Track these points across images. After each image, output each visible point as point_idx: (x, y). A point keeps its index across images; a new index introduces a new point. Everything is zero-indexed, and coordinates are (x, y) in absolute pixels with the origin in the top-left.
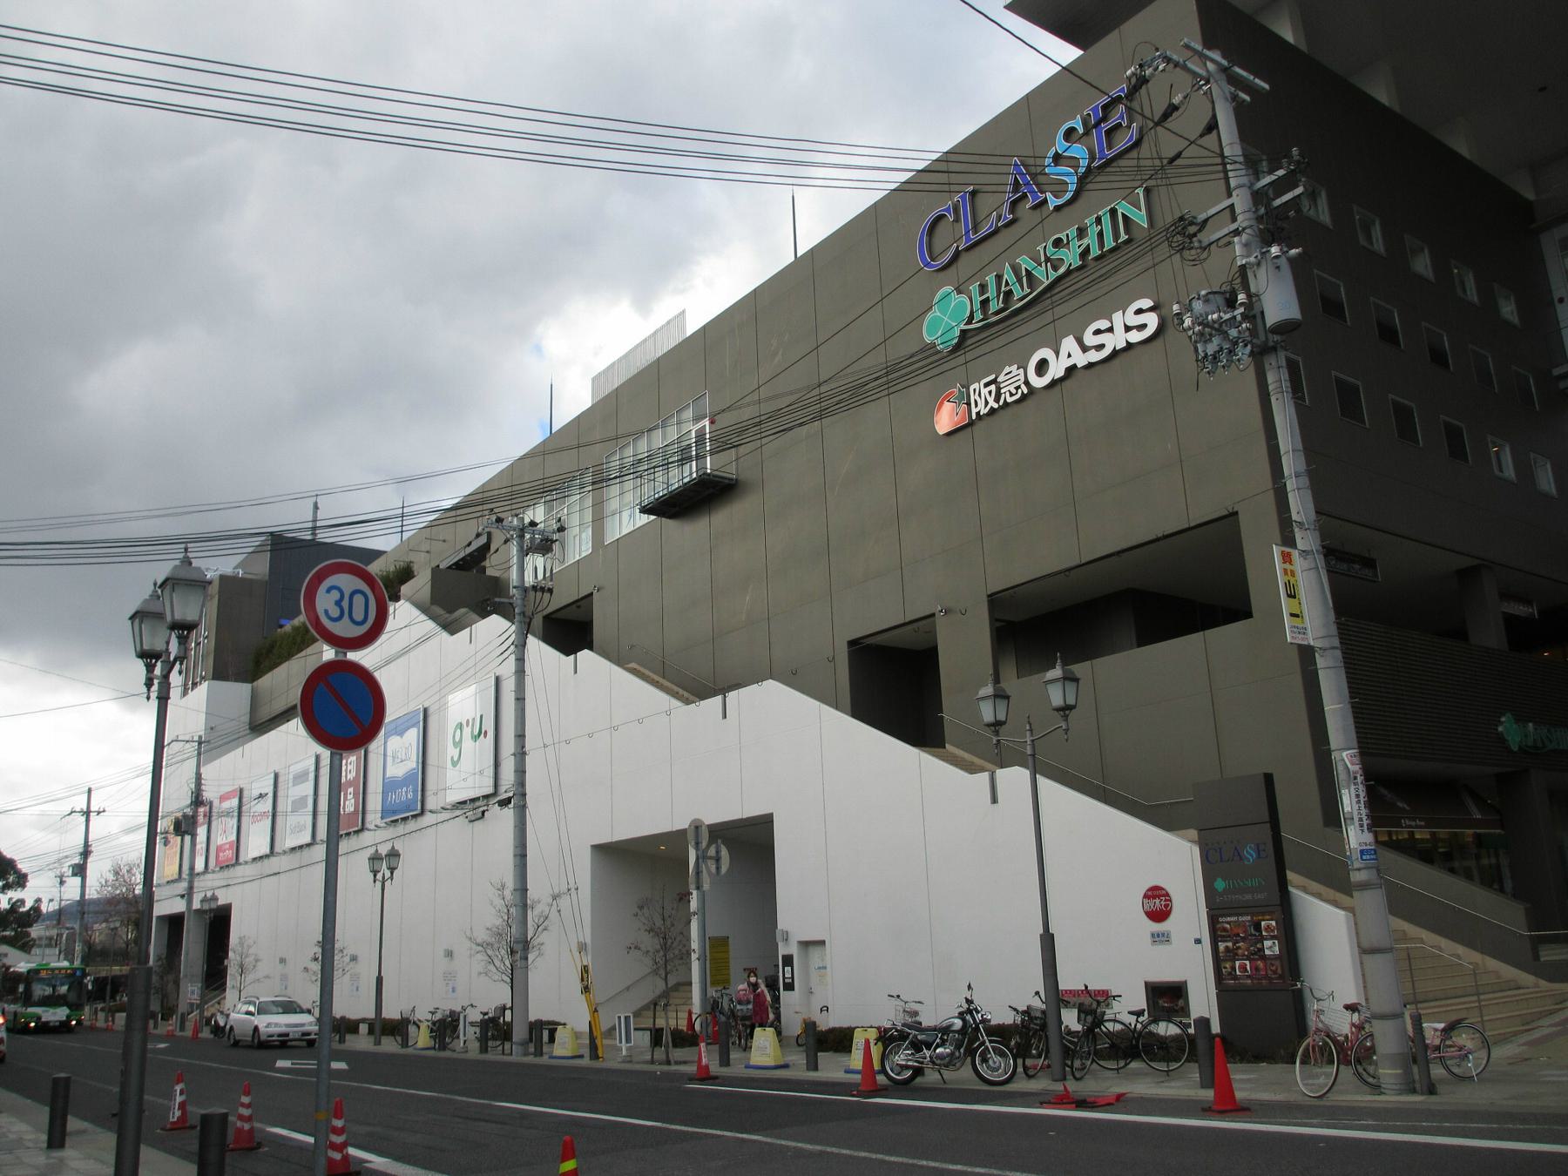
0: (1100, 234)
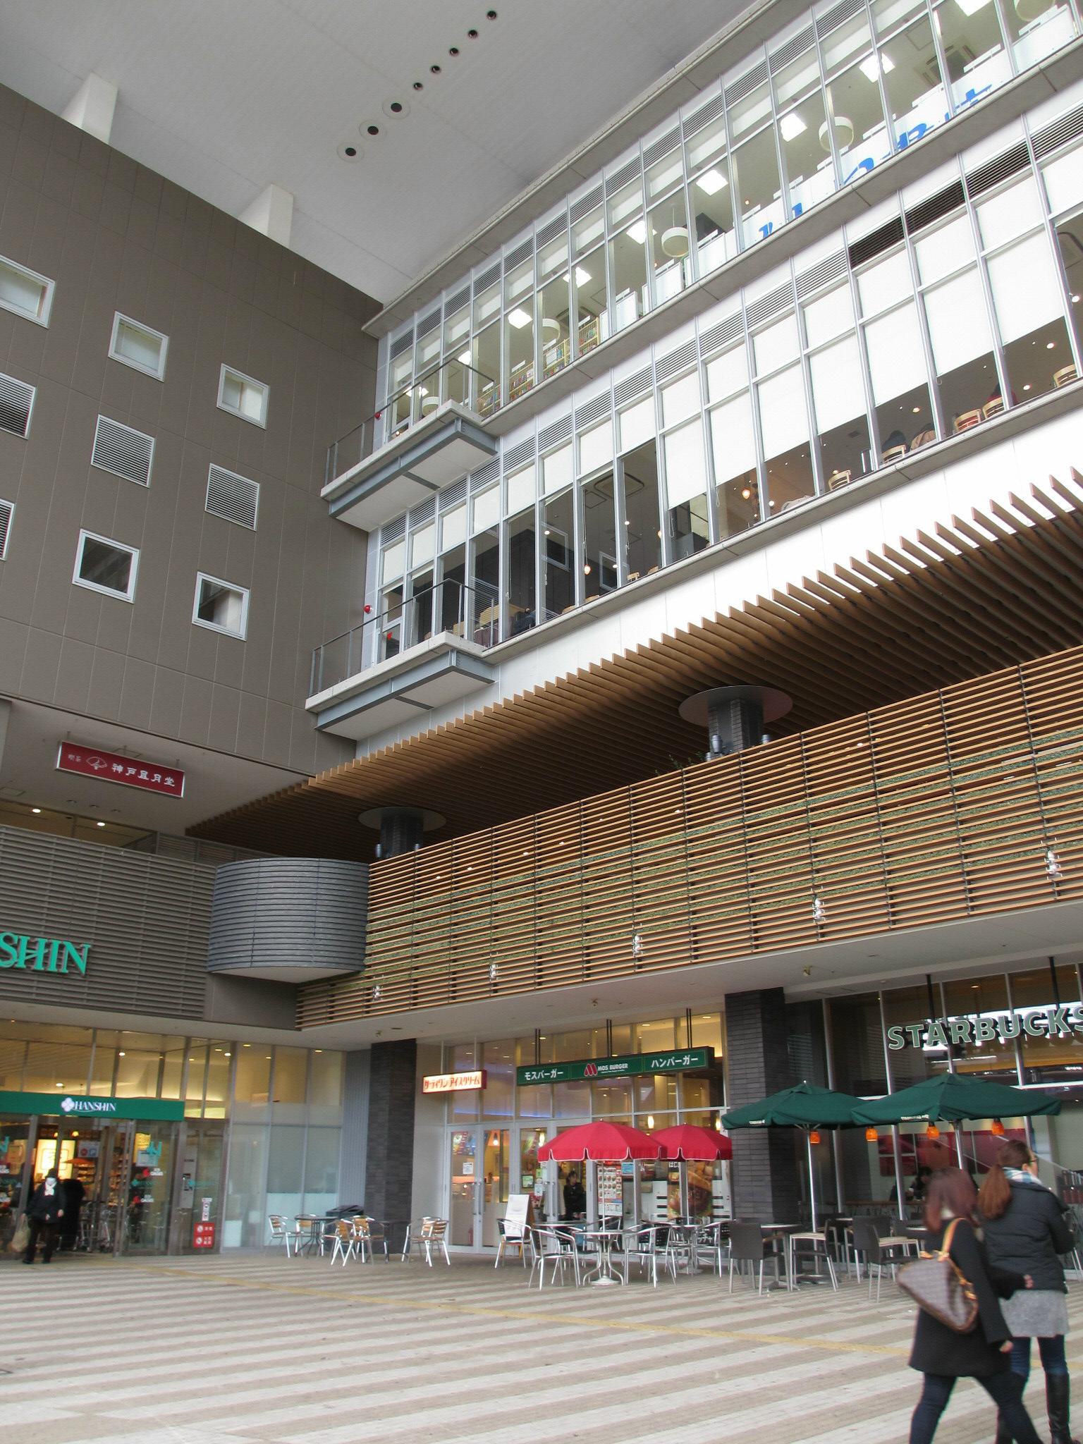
0: (46, 957)
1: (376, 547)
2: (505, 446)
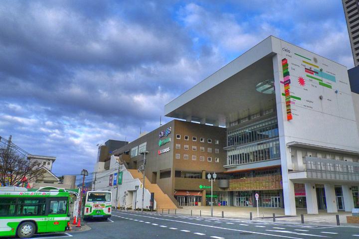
1: (228, 152)
2: (237, 148)
